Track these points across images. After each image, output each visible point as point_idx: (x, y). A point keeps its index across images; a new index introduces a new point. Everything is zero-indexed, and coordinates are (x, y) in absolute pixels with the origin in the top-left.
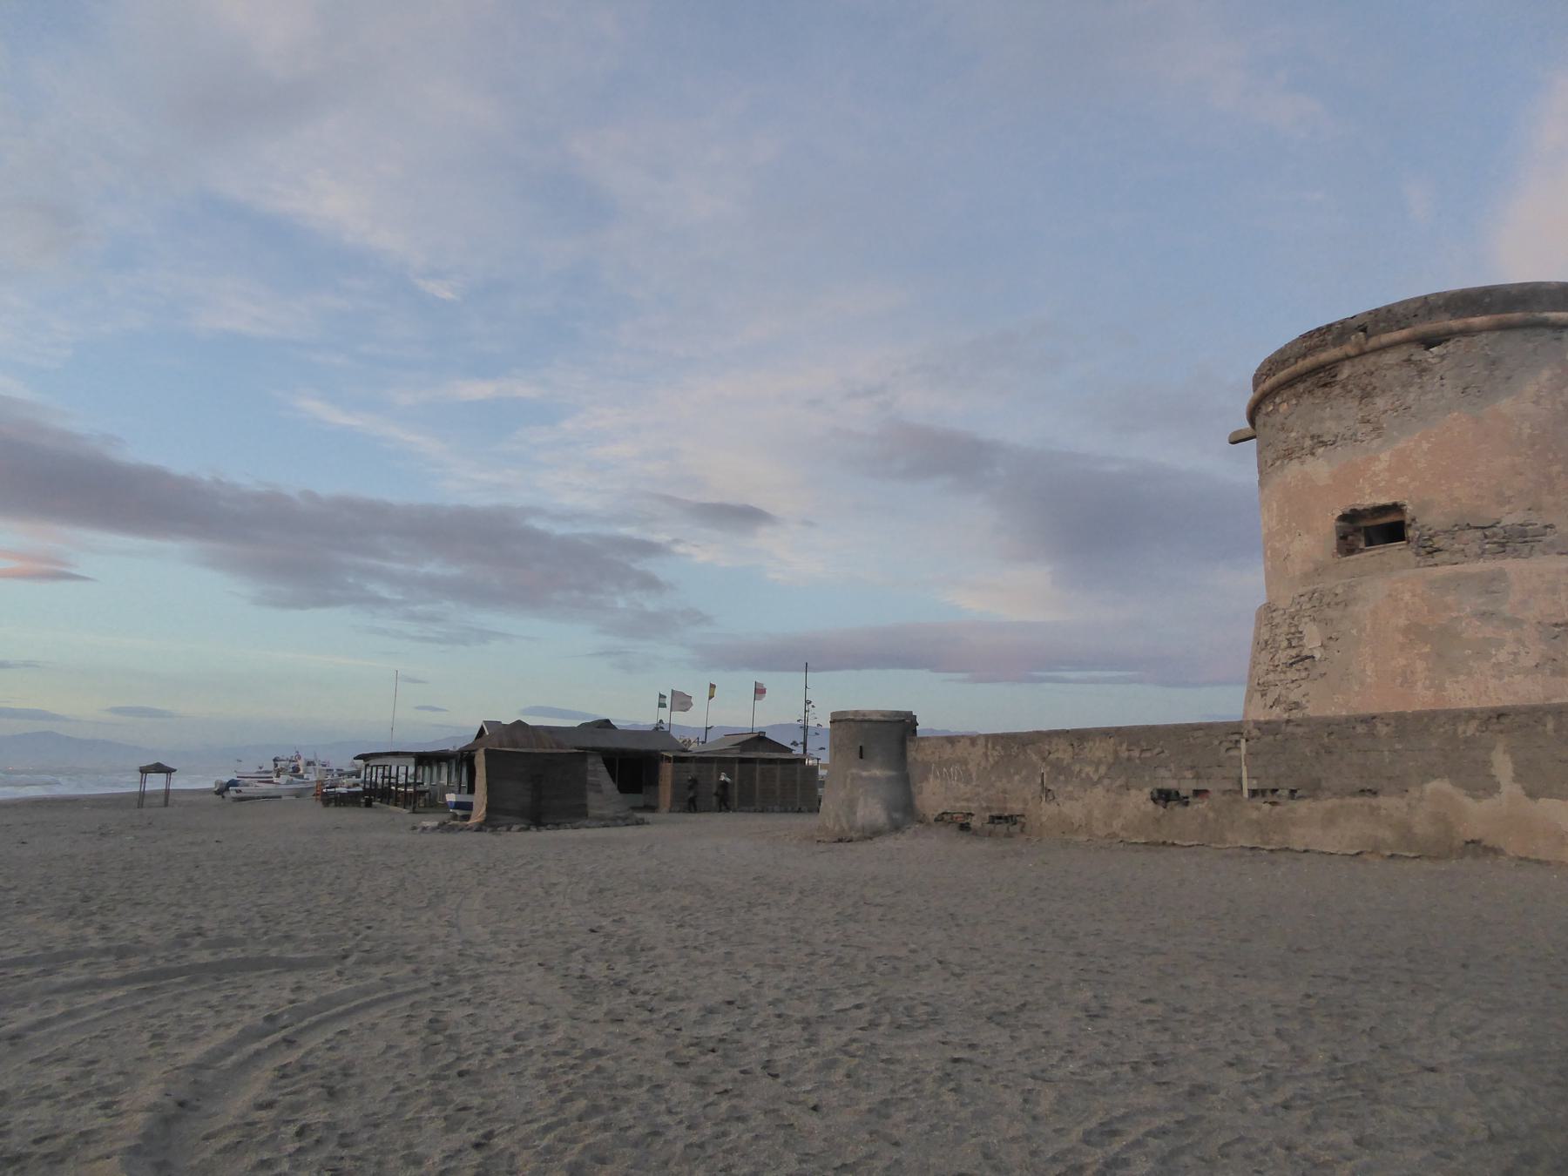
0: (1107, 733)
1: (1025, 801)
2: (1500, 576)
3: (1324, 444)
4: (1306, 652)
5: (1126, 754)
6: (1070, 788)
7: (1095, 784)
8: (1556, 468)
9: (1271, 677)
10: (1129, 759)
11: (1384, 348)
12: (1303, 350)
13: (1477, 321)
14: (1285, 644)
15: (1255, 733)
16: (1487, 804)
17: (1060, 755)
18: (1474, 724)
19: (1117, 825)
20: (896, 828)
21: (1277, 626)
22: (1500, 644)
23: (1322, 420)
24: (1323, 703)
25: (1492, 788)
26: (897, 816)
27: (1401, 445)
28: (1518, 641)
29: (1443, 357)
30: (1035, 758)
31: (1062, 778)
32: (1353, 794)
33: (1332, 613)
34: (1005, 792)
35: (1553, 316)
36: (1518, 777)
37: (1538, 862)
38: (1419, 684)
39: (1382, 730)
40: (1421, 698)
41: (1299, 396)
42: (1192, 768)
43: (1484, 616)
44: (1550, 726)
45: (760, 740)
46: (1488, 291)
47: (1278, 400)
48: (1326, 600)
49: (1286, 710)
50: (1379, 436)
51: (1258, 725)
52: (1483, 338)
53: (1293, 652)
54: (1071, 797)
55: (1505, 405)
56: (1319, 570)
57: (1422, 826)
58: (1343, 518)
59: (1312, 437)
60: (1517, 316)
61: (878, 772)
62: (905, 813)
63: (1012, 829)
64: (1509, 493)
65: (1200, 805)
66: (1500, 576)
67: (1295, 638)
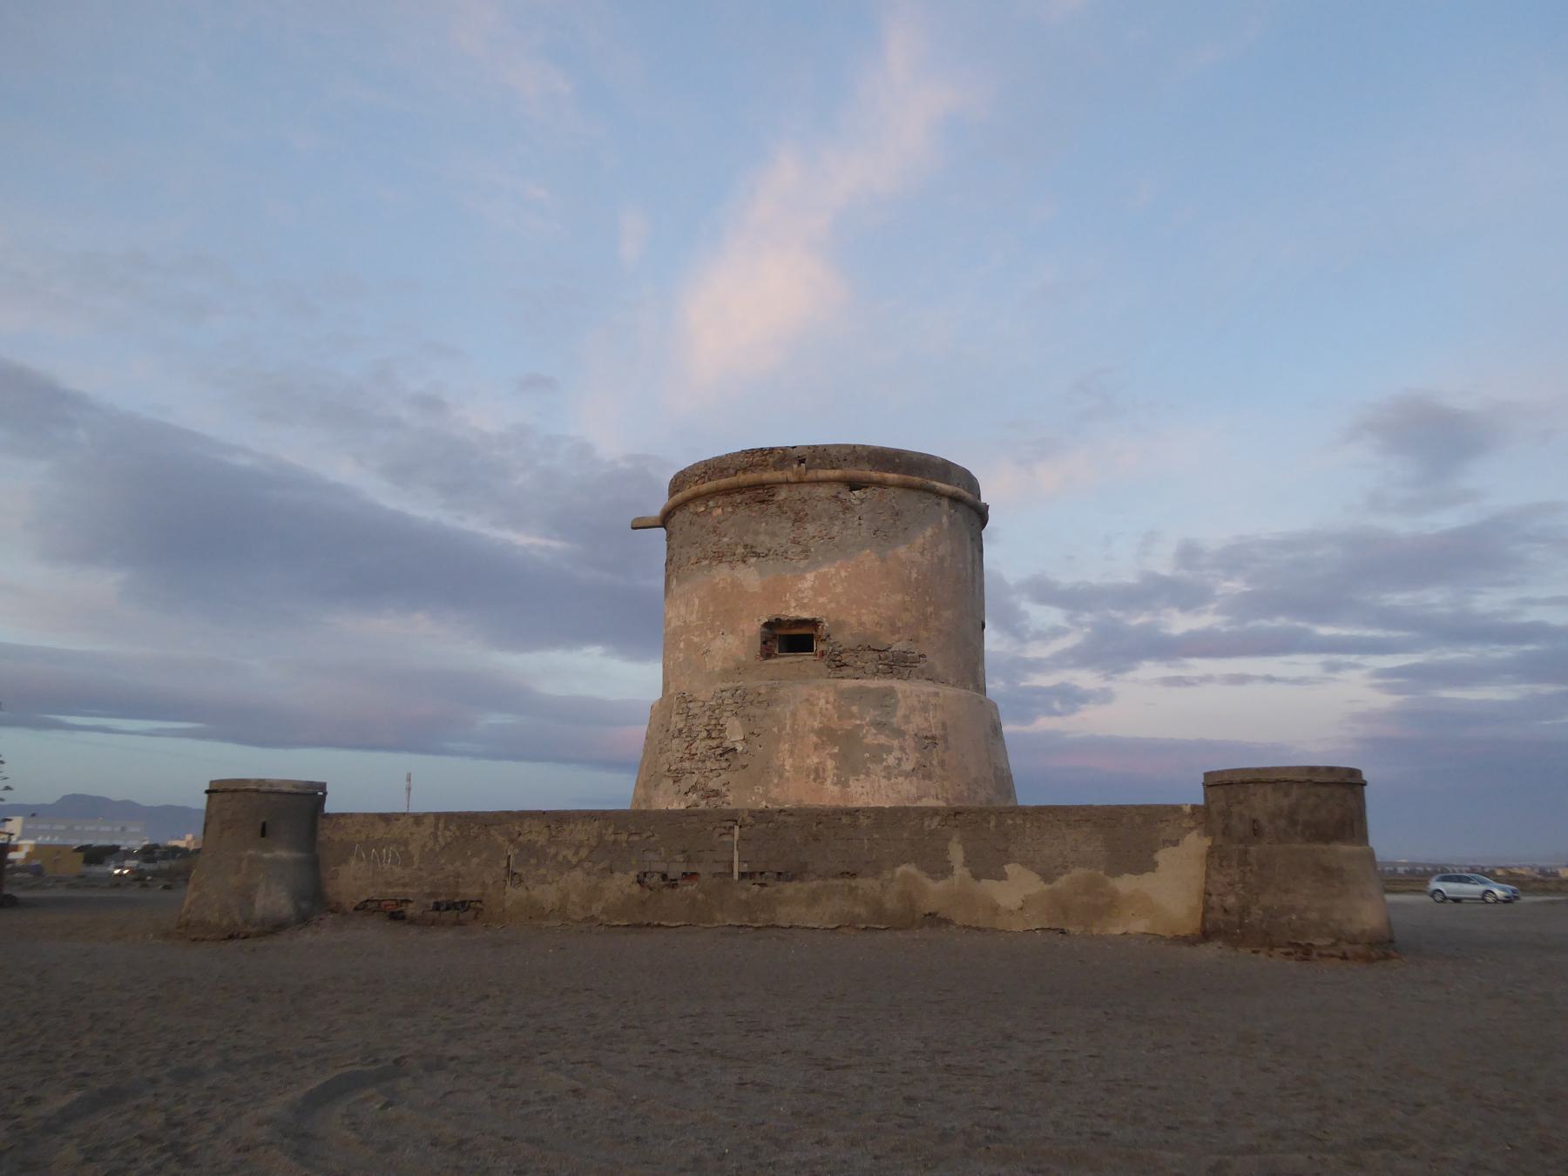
0: (591, 816)
1: (484, 885)
2: (890, 693)
3: (758, 555)
4: (727, 744)
5: (612, 838)
6: (542, 871)
7: (574, 867)
8: (930, 609)
9: (687, 765)
10: (615, 842)
11: (819, 482)
12: (744, 465)
13: (891, 476)
14: (704, 734)
15: (749, 820)
16: (941, 885)
17: (533, 837)
18: (937, 820)
19: (596, 909)
20: (304, 919)
21: (694, 716)
22: (889, 750)
23: (757, 533)
24: (743, 797)
25: (947, 871)
26: (304, 905)
27: (825, 570)
28: (902, 749)
29: (862, 501)
30: (500, 839)
31: (533, 861)
32: (835, 877)
33: (752, 710)
34: (458, 875)
35: (939, 485)
36: (968, 862)
37: (979, 929)
38: (829, 781)
39: (864, 821)
40: (830, 795)
41: (735, 506)
42: (683, 852)
43: (880, 726)
44: (993, 823)
45: (1542, 871)
46: (898, 453)
47: (711, 503)
48: (749, 698)
49: (703, 798)
50: (806, 557)
51: (752, 813)
52: (891, 492)
53: (714, 743)
54: (543, 881)
55: (902, 551)
56: (740, 669)
57: (891, 903)
58: (766, 625)
59: (746, 546)
60: (917, 480)
61: (283, 854)
62: (316, 903)
63: (462, 916)
64: (899, 624)
65: (690, 888)
66: (890, 693)
67: (715, 731)
